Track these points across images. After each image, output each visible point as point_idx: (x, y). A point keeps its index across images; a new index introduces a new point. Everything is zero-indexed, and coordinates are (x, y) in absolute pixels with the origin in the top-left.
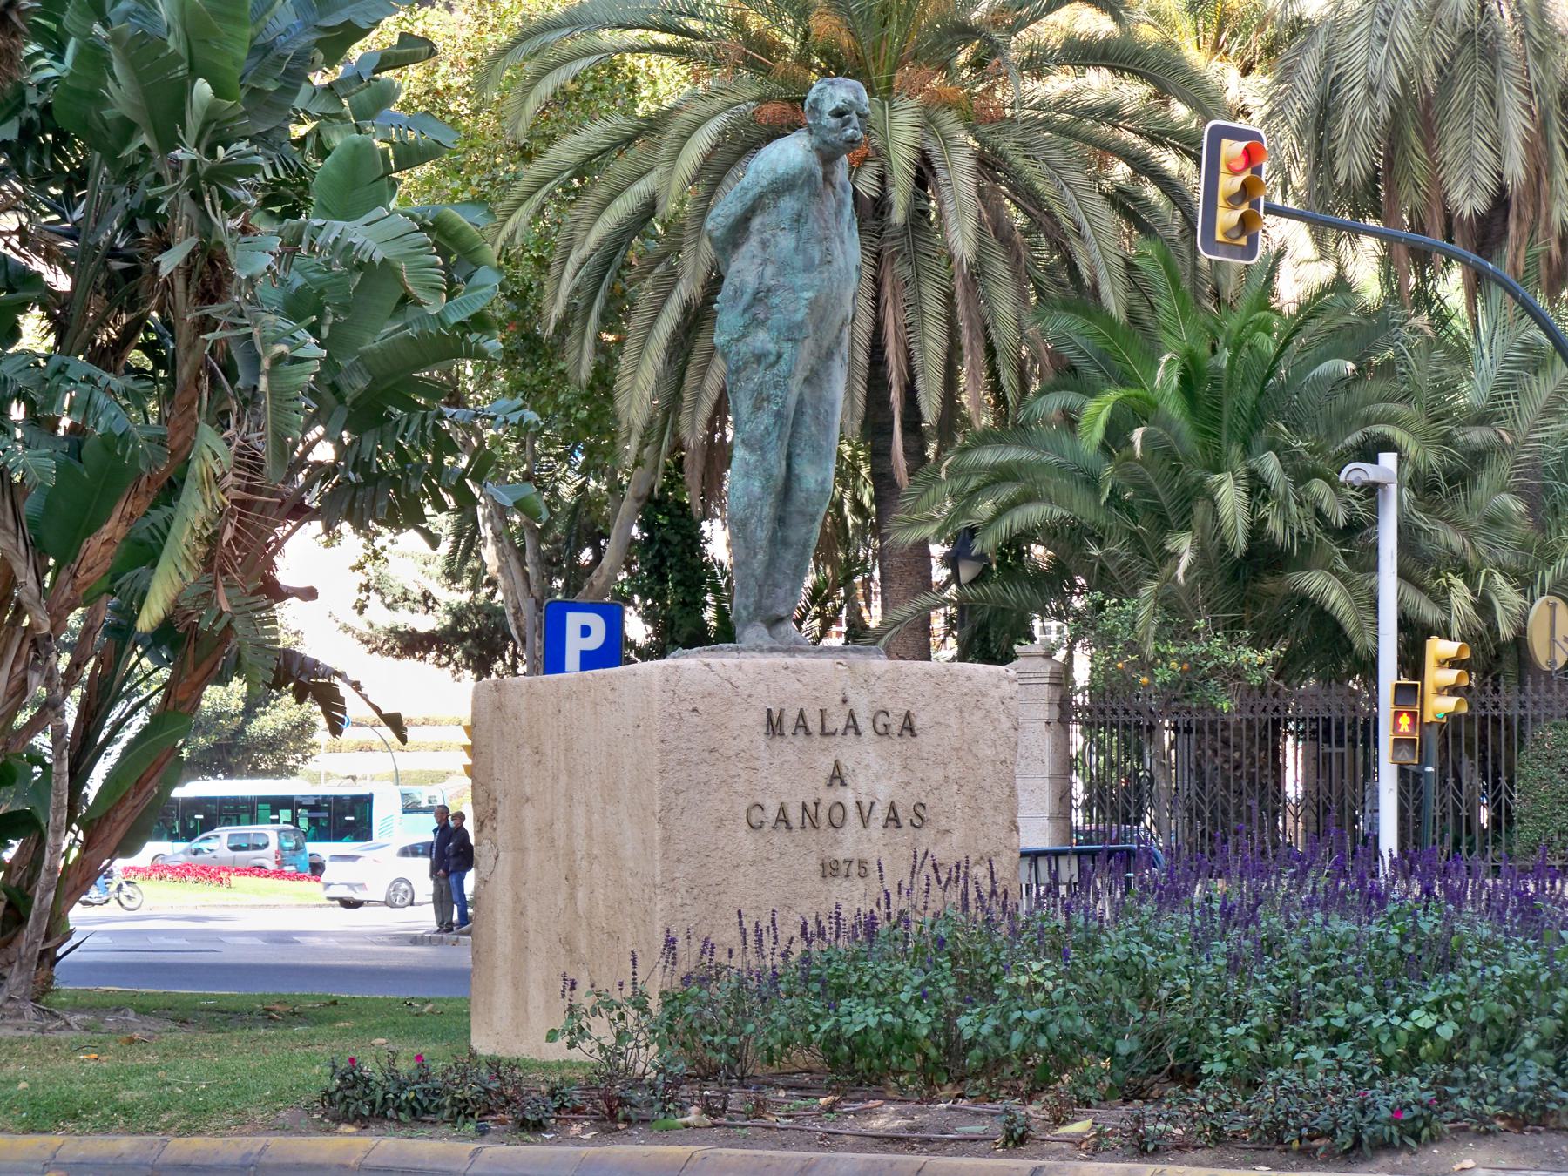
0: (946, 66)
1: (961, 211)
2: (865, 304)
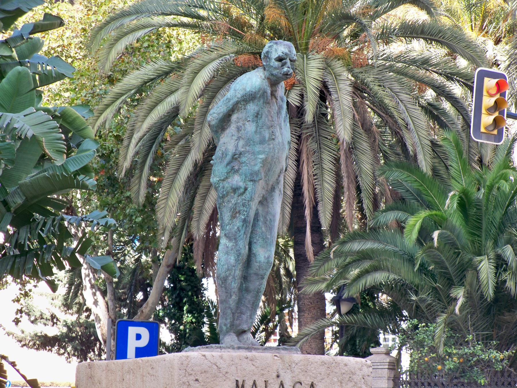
0: (337, 37)
1: (343, 114)
2: (292, 163)
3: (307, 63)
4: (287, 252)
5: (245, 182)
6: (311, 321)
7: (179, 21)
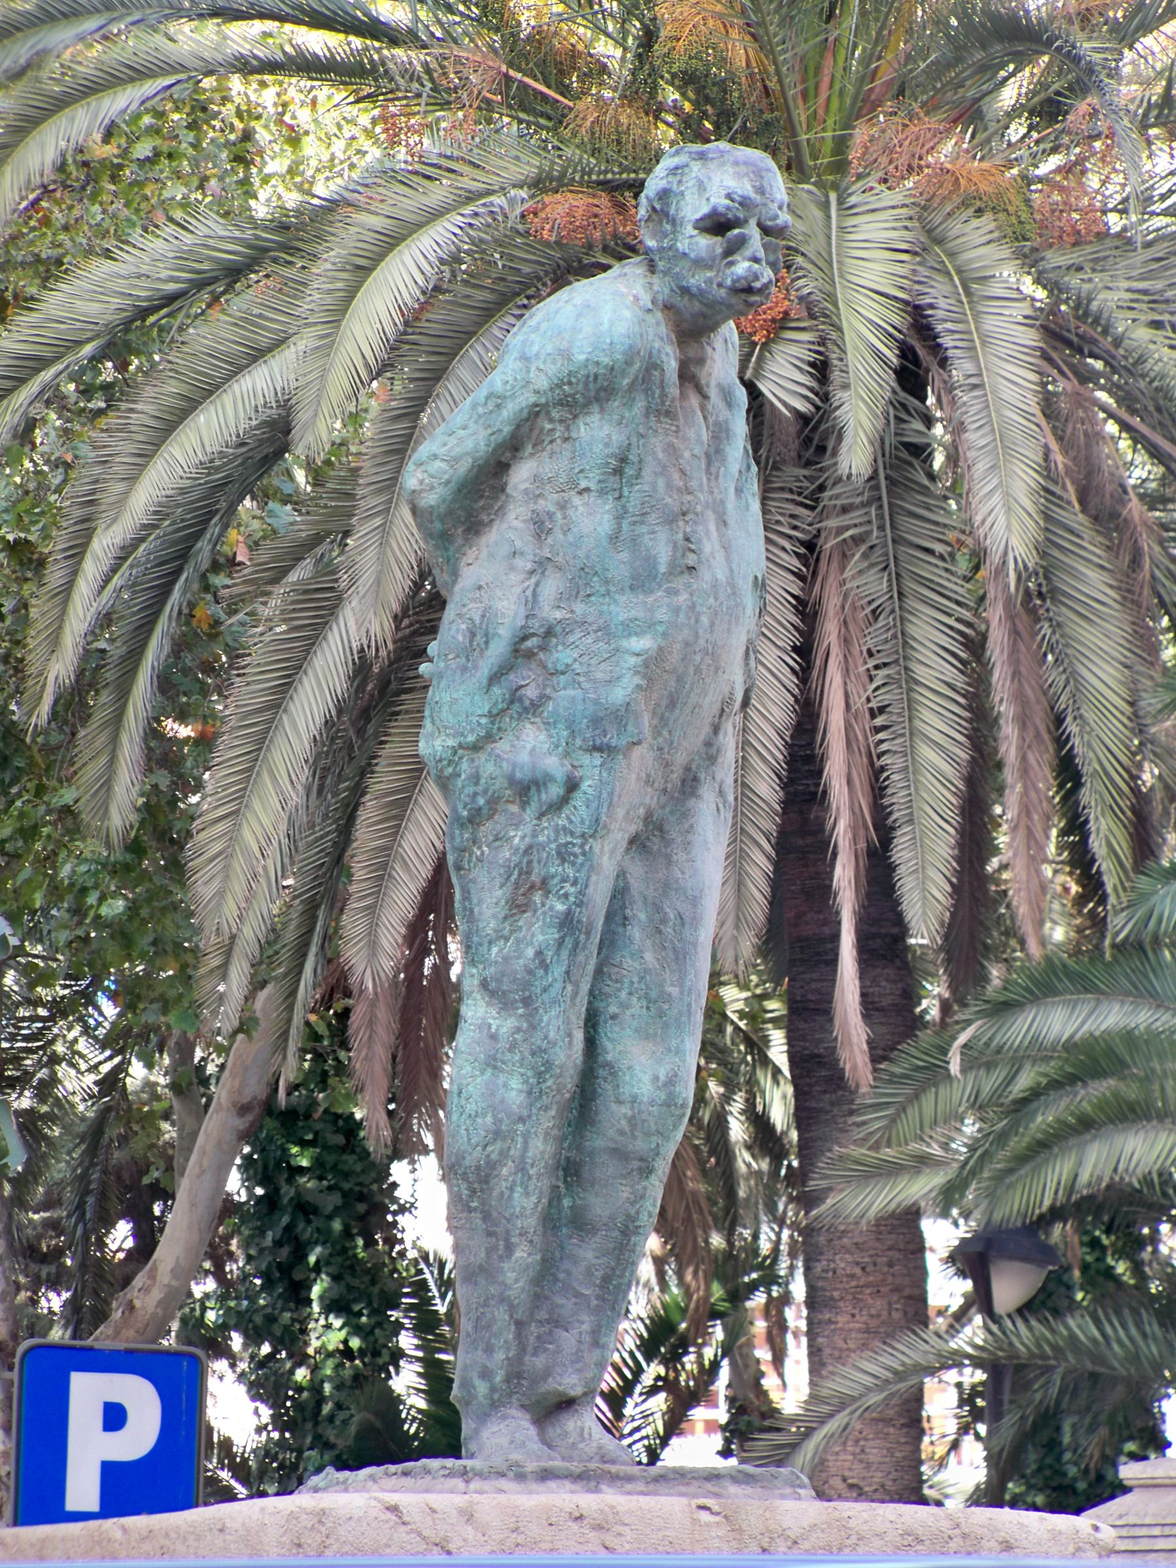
0: (970, 114)
1: (1003, 447)
2: (776, 662)
3: (842, 229)
4: (757, 1046)
5: (567, 754)
6: (864, 1346)
7: (288, 49)
